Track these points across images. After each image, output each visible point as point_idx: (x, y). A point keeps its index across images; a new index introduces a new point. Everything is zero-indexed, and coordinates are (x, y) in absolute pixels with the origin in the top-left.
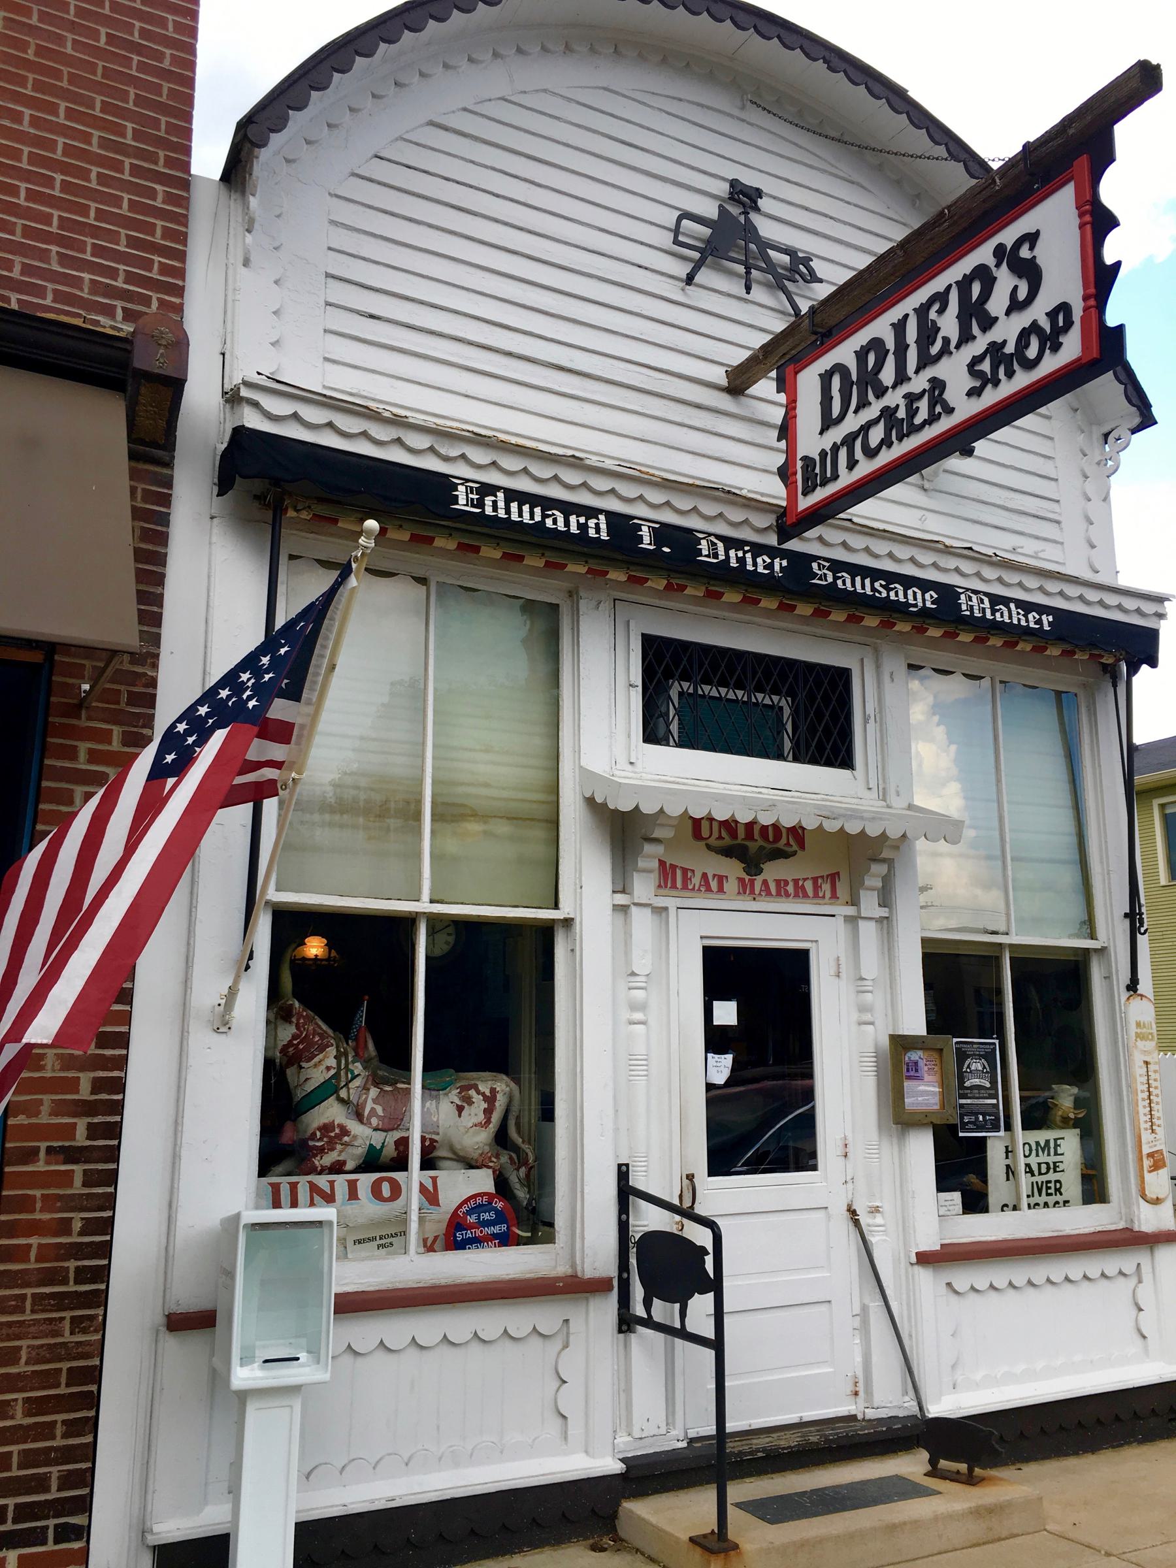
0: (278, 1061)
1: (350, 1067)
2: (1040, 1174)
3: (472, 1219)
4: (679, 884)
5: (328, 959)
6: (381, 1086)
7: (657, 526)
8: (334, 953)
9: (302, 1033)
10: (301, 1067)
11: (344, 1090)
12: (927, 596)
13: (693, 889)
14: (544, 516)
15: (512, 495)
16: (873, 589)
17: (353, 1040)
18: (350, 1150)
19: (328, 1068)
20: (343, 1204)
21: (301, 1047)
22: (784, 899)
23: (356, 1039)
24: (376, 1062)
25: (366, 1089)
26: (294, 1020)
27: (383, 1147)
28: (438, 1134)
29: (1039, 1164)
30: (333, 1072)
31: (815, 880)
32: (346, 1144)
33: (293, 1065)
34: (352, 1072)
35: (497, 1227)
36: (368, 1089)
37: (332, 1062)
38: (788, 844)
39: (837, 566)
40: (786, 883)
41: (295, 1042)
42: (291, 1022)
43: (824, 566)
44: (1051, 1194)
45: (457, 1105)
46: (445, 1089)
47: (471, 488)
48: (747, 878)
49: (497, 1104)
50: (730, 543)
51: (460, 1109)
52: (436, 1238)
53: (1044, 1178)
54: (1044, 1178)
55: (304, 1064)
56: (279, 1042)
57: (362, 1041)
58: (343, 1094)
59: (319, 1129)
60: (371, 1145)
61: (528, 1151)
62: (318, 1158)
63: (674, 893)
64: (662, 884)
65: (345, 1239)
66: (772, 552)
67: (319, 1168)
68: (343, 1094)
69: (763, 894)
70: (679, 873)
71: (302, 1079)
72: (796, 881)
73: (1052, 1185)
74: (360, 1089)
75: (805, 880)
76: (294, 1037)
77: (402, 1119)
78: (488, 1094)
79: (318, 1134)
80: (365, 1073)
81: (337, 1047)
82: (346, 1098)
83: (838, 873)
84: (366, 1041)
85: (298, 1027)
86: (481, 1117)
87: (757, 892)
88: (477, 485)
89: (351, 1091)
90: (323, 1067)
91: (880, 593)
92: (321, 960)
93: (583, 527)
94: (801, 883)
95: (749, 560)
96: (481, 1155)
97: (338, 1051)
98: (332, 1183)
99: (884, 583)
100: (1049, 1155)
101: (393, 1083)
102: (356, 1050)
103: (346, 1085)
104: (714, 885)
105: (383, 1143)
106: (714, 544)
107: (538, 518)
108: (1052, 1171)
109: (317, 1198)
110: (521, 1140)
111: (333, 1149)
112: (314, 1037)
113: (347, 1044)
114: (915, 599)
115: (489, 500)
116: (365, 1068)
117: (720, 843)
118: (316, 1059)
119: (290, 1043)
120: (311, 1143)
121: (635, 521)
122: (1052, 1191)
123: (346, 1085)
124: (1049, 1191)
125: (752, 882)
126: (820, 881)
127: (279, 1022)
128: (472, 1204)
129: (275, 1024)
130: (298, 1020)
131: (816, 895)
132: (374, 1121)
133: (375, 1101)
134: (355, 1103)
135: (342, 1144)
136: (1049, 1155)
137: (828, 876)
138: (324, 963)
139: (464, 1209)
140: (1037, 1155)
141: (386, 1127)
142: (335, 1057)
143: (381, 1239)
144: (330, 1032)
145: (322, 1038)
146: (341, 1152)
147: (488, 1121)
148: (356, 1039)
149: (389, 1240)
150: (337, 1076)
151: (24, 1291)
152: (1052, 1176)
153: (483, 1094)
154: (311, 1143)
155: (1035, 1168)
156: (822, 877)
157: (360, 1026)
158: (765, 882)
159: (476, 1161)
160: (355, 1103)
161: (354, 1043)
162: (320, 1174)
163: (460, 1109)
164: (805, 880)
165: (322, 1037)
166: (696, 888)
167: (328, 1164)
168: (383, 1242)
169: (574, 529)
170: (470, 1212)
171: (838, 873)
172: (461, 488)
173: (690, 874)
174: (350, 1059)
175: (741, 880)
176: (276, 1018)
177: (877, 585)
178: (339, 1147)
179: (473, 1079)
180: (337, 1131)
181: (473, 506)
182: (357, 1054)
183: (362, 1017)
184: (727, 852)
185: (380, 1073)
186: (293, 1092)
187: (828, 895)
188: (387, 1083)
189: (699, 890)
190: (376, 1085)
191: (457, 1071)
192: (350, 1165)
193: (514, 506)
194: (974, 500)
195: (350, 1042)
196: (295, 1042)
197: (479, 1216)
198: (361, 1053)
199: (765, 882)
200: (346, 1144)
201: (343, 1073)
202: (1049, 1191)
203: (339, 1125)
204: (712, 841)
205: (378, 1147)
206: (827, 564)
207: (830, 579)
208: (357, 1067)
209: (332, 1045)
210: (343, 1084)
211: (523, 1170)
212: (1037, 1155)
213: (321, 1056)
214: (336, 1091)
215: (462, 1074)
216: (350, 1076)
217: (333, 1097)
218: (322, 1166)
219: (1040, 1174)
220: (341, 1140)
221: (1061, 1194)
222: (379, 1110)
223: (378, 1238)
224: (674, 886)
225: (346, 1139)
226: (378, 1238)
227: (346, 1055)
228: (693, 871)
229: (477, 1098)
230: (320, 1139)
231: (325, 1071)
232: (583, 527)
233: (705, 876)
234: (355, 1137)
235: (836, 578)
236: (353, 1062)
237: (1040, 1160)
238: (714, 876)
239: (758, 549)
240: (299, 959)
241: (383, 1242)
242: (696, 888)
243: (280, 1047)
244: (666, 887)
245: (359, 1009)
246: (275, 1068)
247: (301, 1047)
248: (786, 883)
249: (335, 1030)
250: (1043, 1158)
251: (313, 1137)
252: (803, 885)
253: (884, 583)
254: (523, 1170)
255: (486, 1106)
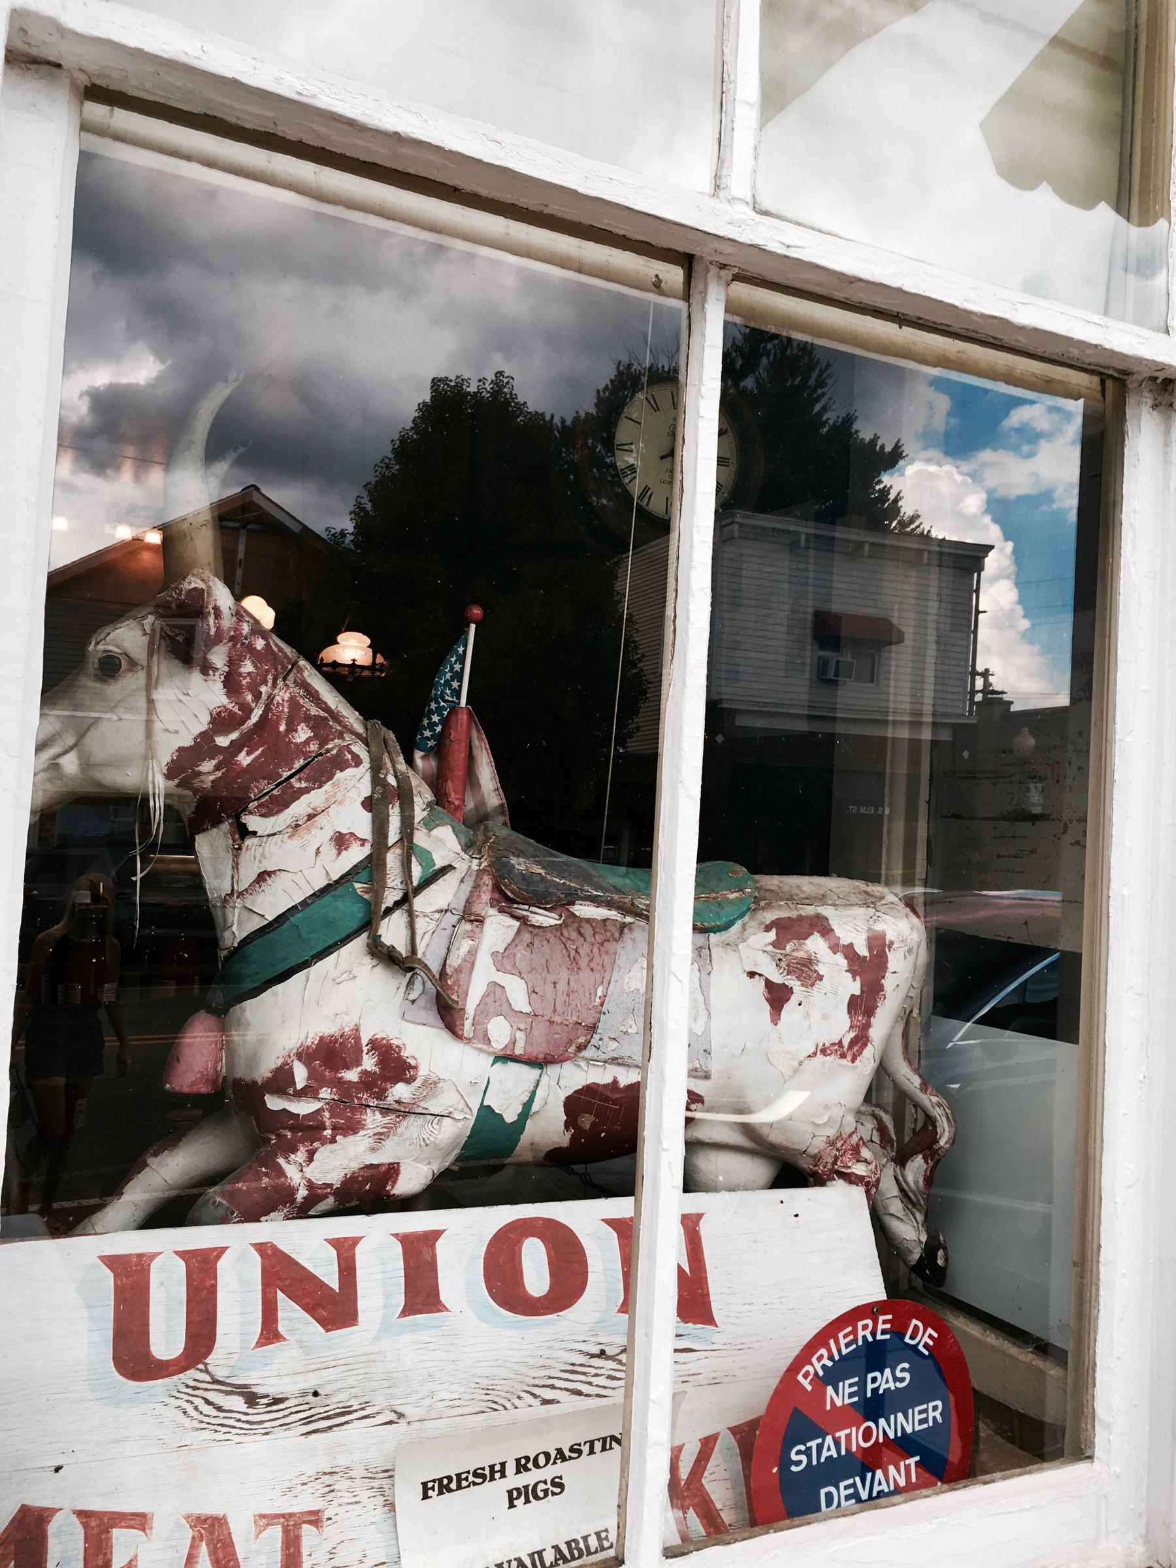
0: (158, 805)
1: (421, 838)
3: (841, 1396)
5: (373, 667)
6: (522, 910)
8: (380, 659)
9: (247, 711)
10: (244, 832)
11: (399, 917)
17: (428, 752)
18: (411, 1128)
19: (341, 841)
20: (385, 1328)
21: (244, 759)
23: (439, 751)
24: (500, 829)
25: (471, 916)
26: (218, 658)
27: (526, 1112)
28: (707, 1077)
30: (356, 854)
32: (402, 1111)
33: (217, 822)
34: (426, 858)
35: (916, 1413)
36: (480, 921)
37: (361, 823)
41: (223, 741)
42: (206, 669)
45: (769, 984)
46: (727, 927)
49: (889, 982)
51: (777, 997)
52: (708, 1444)
55: (252, 822)
56: (160, 737)
57: (458, 757)
58: (393, 932)
59: (305, 1055)
60: (486, 1112)
61: (937, 1112)
62: (300, 1156)
65: (389, 1474)
67: (302, 1193)
68: (393, 932)
71: (248, 875)
74: (451, 919)
76: (221, 722)
77: (593, 1028)
78: (862, 950)
79: (301, 1075)
80: (466, 865)
81: (376, 768)
82: (402, 949)
84: (471, 759)
85: (231, 683)
86: (841, 1027)
89: (421, 924)
90: (320, 835)
92: (363, 667)
96: (832, 1143)
97: (377, 780)
98: (345, 1250)
101: (562, 902)
102: (437, 783)
103: (404, 901)
105: (527, 1105)
109: (289, 1312)
110: (917, 1081)
111: (351, 1128)
112: (291, 729)
113: (410, 762)
116: (468, 847)
118: (300, 808)
119: (203, 746)
120: (274, 1103)
123: (404, 901)
127: (164, 666)
128: (843, 1345)
129: (149, 668)
130: (233, 663)
132: (500, 1032)
133: (503, 960)
134: (435, 968)
135: (385, 1111)
138: (366, 673)
139: (818, 1364)
141: (539, 1050)
142: (368, 804)
143: (521, 1467)
144: (352, 718)
145: (317, 725)
146: (380, 1137)
147: (861, 1040)
148: (439, 751)
149: (549, 1472)
150: (372, 867)
151: (800, 529)
153: (849, 952)
154: (274, 1103)
157: (454, 709)
159: (817, 1158)
160: (435, 968)
161: (433, 763)
162: (303, 1212)
163: (777, 997)
165: (322, 726)
167: (335, 1178)
168: (529, 1478)
170: (832, 1377)
174: (419, 813)
176: (151, 652)
178: (373, 1120)
179: (810, 900)
180: (369, 1063)
182: (440, 798)
183: (459, 676)
185: (519, 864)
186: (218, 914)
188: (541, 900)
190: (505, 901)
191: (754, 870)
192: (409, 1182)
195: (418, 755)
196: (223, 741)
197: (862, 1385)
198: (454, 797)
200: (402, 1111)
201: (392, 860)
203: (375, 1044)
205: (510, 1117)
208: (442, 842)
209: (358, 762)
210: (391, 897)
211: (916, 1167)
213: (315, 798)
214: (368, 924)
215: (772, 882)
216: (417, 872)
217: (360, 944)
218: (310, 1185)
220: (381, 1095)
222: (517, 993)
223: (511, 1468)
225: (400, 1091)
226: (511, 1468)
227: (405, 796)
229: (832, 965)
230: (309, 1092)
231: (329, 850)
234: (432, 1084)
236: (429, 824)
240: (327, 665)
241: (529, 1478)
243: (165, 754)
245: (439, 660)
246: (146, 822)
247: (244, 759)
249: (366, 713)
251: (281, 1081)
254: (916, 1167)
255: (855, 988)
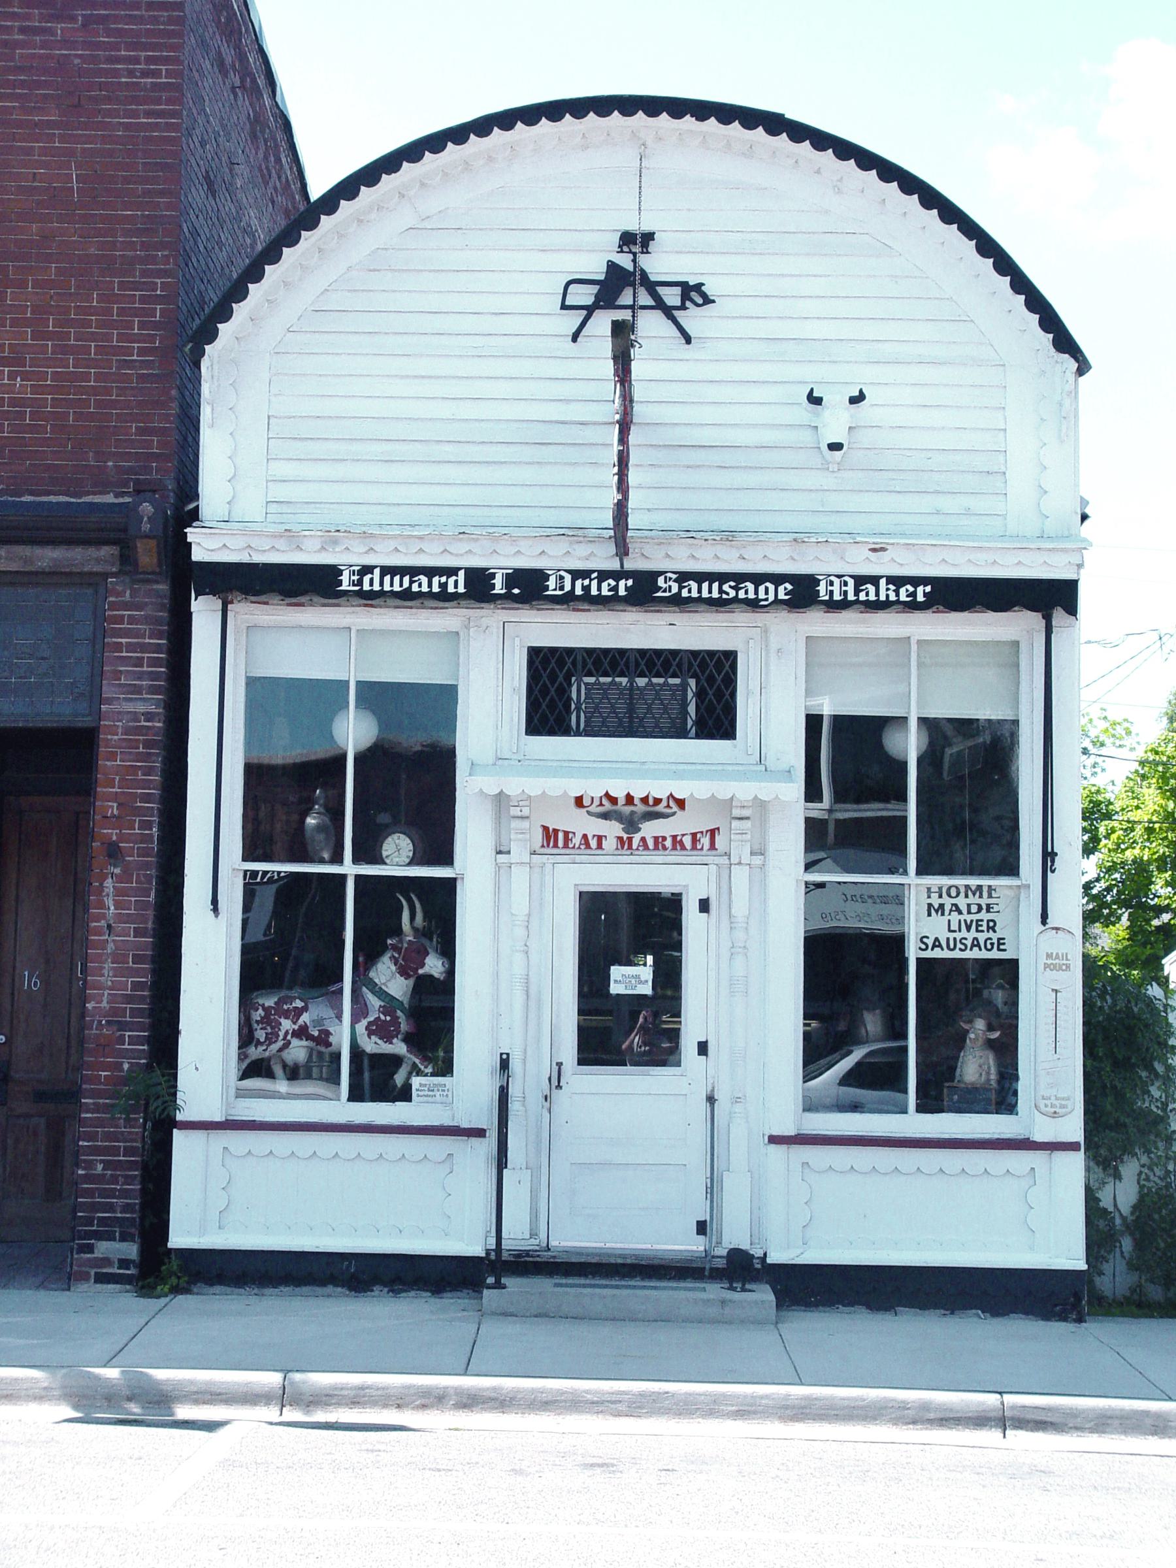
2: (969, 912)
4: (561, 843)
7: (510, 571)
12: (781, 589)
13: (574, 847)
14: (411, 582)
15: (386, 571)
16: (721, 591)
22: (661, 852)
29: (969, 905)
31: (694, 835)
38: (668, 806)
39: (683, 577)
40: (664, 839)
43: (670, 579)
44: (982, 931)
47: (354, 571)
48: (625, 836)
50: (576, 574)
53: (978, 917)
54: (978, 917)
63: (555, 851)
64: (545, 844)
66: (618, 575)
69: (641, 848)
70: (561, 835)
72: (674, 837)
73: (985, 924)
75: (683, 835)
83: (718, 829)
87: (634, 847)
88: (359, 568)
91: (727, 594)
93: (444, 586)
94: (679, 838)
95: (594, 584)
99: (732, 584)
100: (981, 896)
104: (593, 843)
106: (562, 578)
107: (406, 584)
108: (984, 911)
114: (767, 593)
115: (366, 579)
117: (600, 809)
121: (492, 571)
122: (984, 928)
124: (980, 928)
125: (630, 840)
126: (699, 836)
131: (694, 848)
136: (981, 896)
137: (707, 831)
140: (967, 896)
152: (984, 915)
155: (964, 909)
156: (702, 832)
158: (643, 839)
164: (683, 835)
166: (577, 846)
169: (436, 589)
171: (718, 829)
172: (346, 574)
173: (571, 835)
175: (620, 839)
177: (726, 587)
181: (354, 585)
184: (605, 816)
187: (707, 845)
189: (579, 848)
193: (387, 579)
194: (445, 462)
199: (643, 839)
202: (980, 928)
204: (593, 809)
206: (674, 576)
207: (675, 589)
212: (967, 896)
219: (969, 912)
221: (995, 931)
224: (556, 846)
228: (574, 833)
232: (444, 586)
233: (585, 836)
235: (681, 588)
237: (968, 901)
238: (594, 836)
239: (603, 575)
242: (577, 846)
244: (548, 846)
248: (664, 839)
250: (972, 899)
252: (681, 840)
253: (732, 584)
